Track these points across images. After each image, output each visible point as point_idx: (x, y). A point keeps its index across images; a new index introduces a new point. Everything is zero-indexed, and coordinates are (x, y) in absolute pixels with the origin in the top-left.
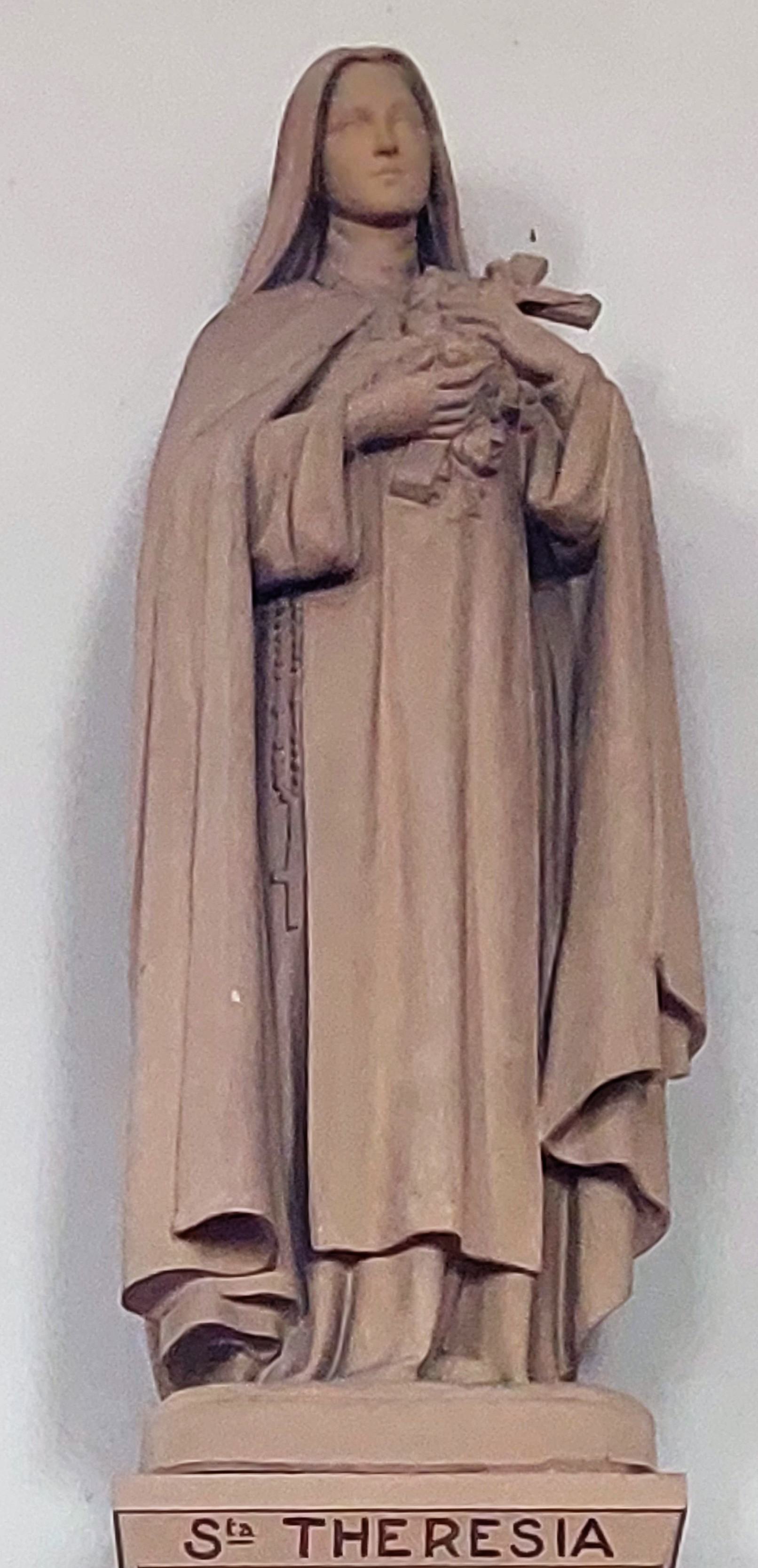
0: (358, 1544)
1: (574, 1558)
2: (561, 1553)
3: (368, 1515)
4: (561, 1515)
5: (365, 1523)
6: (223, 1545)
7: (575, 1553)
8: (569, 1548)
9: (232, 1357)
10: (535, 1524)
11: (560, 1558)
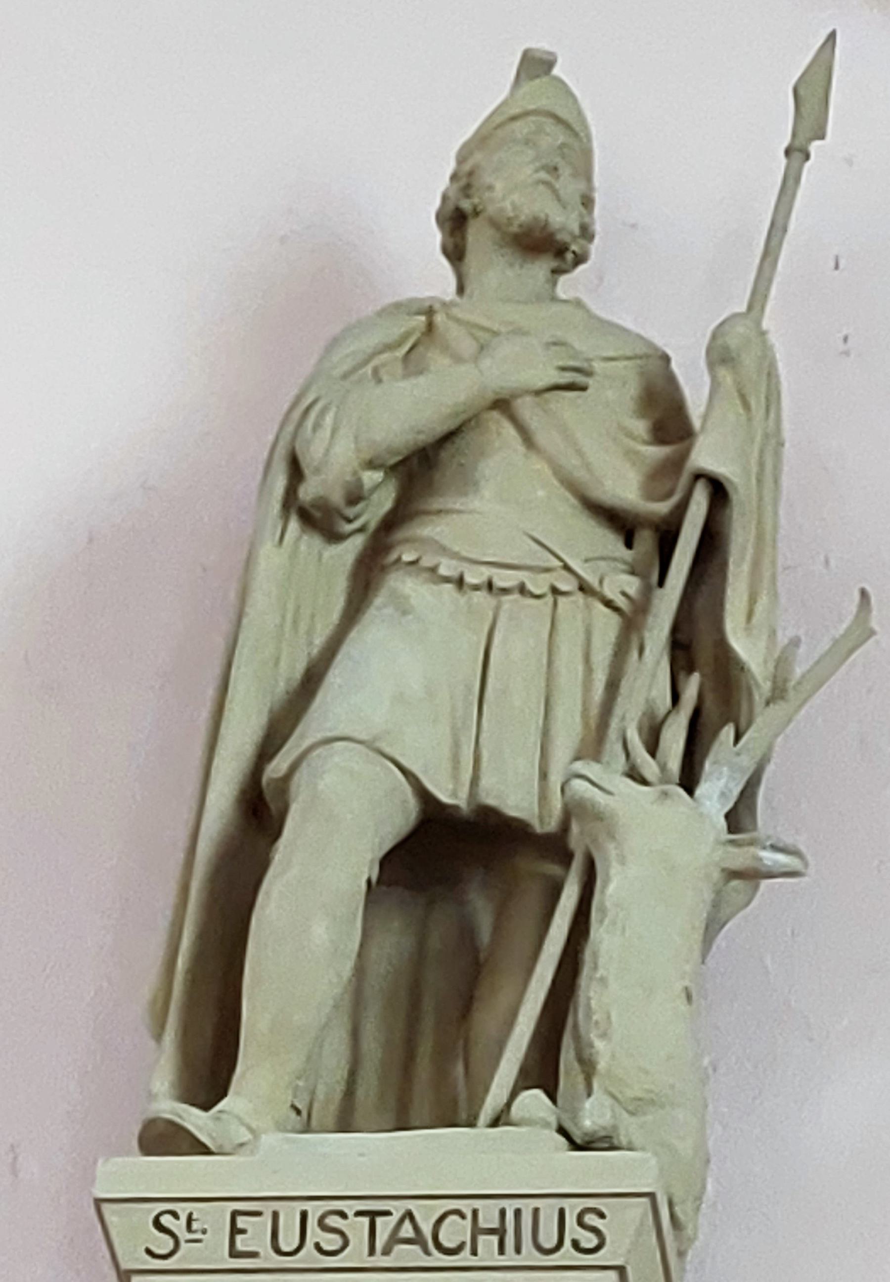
0: (495, 1239)
1: (385, 1258)
2: (372, 1251)
3: (308, 1206)
4: (411, 1205)
5: (503, 1213)
6: (183, 1245)
7: (386, 1252)
8: (379, 1244)
9: (593, 1051)
10: (602, 1216)
11: (517, 1257)
